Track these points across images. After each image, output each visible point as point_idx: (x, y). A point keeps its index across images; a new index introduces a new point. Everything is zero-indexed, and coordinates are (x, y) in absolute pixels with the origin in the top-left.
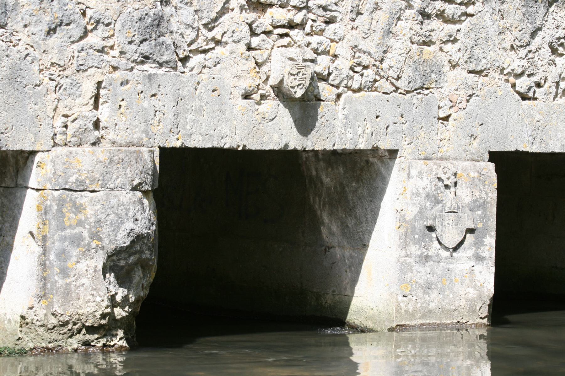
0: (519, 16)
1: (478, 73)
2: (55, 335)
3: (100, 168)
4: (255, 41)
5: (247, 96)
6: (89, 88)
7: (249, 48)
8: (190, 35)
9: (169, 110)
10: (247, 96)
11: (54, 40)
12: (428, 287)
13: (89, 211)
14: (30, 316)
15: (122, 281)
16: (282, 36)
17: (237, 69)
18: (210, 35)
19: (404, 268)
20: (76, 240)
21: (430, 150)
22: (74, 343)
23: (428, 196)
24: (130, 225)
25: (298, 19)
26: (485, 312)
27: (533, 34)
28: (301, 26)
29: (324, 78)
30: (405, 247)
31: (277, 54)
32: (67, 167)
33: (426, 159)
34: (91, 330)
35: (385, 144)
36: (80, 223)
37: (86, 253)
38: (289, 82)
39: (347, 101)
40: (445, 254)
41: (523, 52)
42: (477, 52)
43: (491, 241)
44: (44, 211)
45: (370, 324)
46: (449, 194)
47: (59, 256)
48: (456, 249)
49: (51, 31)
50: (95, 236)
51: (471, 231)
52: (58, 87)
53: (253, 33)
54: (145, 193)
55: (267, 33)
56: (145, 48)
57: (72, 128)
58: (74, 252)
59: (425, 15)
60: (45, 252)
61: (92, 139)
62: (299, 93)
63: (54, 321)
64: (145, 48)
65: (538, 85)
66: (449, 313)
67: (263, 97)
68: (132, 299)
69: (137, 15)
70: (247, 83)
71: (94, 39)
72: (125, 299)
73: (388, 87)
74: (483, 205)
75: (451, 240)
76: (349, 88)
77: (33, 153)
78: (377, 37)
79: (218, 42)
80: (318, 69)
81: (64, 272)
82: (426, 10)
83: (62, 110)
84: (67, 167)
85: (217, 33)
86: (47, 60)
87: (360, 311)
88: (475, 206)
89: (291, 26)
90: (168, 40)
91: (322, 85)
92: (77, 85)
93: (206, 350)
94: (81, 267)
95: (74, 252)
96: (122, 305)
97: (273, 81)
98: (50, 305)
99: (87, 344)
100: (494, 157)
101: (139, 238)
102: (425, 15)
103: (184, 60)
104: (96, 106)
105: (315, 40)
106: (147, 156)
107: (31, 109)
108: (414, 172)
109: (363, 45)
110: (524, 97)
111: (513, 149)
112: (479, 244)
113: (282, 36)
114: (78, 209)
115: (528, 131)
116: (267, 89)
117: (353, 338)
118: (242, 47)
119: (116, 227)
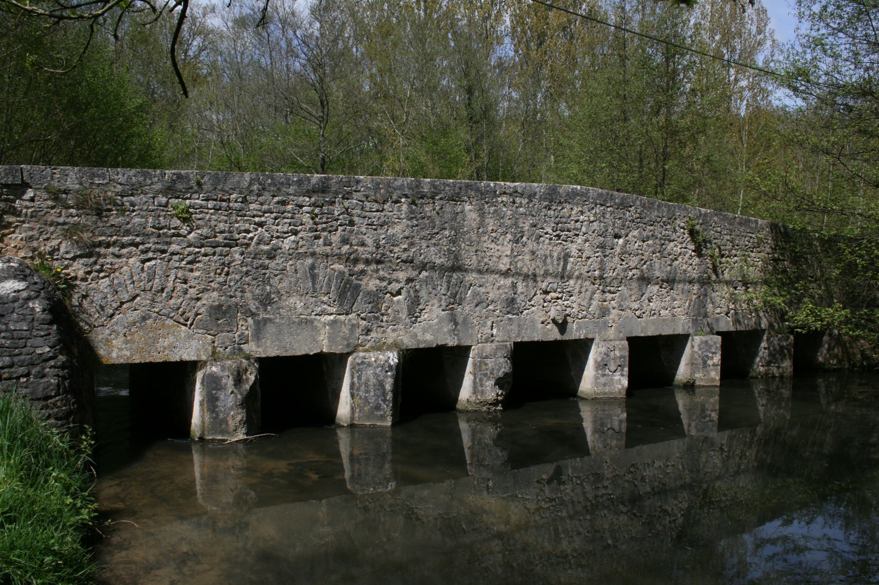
0: (637, 290)
1: (623, 310)
2: (478, 406)
3: (493, 351)
4: (545, 304)
5: (543, 323)
6: (489, 323)
7: (543, 307)
8: (523, 304)
9: (516, 329)
10: (543, 323)
11: (477, 308)
12: (605, 385)
13: (490, 365)
14: (470, 399)
15: (500, 388)
16: (554, 302)
17: (539, 314)
18: (530, 303)
19: (596, 378)
20: (485, 375)
21: (605, 337)
22: (485, 409)
23: (605, 354)
24: (503, 370)
25: (560, 296)
26: (625, 393)
27: (642, 296)
28: (561, 298)
29: (568, 315)
30: (597, 371)
31: (553, 309)
32: (482, 350)
33: (605, 341)
34: (490, 404)
35: (590, 336)
36: (487, 369)
37: (488, 379)
38: (557, 318)
39: (577, 323)
40: (610, 373)
41: (638, 302)
42: (622, 303)
43: (626, 369)
44: (474, 365)
45: (585, 397)
46: (612, 353)
47: (480, 380)
48: (614, 372)
49: (477, 305)
50: (492, 373)
51: (619, 366)
52: (479, 323)
53: (545, 302)
54: (508, 359)
55: (550, 302)
56: (508, 309)
57: (484, 337)
58: (485, 379)
59: (604, 292)
60: (475, 378)
61: (490, 340)
62: (560, 322)
63: (478, 401)
64: (508, 309)
65: (644, 313)
66: (612, 393)
67: (548, 323)
68: (504, 393)
69: (505, 298)
70: (544, 319)
71: (491, 307)
72: (502, 393)
73: (591, 317)
74: (624, 357)
75: (613, 368)
76: (578, 318)
77: (471, 346)
78: (587, 300)
79: (533, 306)
80: (567, 312)
81: (482, 385)
82: (453, 482)
83: (480, 331)
84: (482, 350)
85: (532, 302)
86: (476, 315)
87: (582, 392)
88: (621, 357)
89: (558, 298)
90: (516, 306)
91: (568, 318)
92: (485, 323)
93: (103, 386)
94: (487, 384)
95: (485, 379)
96: (501, 396)
97: (551, 318)
98: (477, 396)
99: (489, 409)
100: (630, 339)
101: (506, 374)
102: (604, 292)
103: (522, 312)
104: (492, 329)
105: (565, 303)
106: (509, 346)
107: (470, 331)
108: (600, 346)
109: (582, 304)
110: (639, 317)
111: (634, 335)
112: (622, 370)
113: (554, 302)
114: (486, 364)
115: (640, 329)
116: (550, 320)
117: (459, 415)
118: (541, 307)
119: (499, 370)
